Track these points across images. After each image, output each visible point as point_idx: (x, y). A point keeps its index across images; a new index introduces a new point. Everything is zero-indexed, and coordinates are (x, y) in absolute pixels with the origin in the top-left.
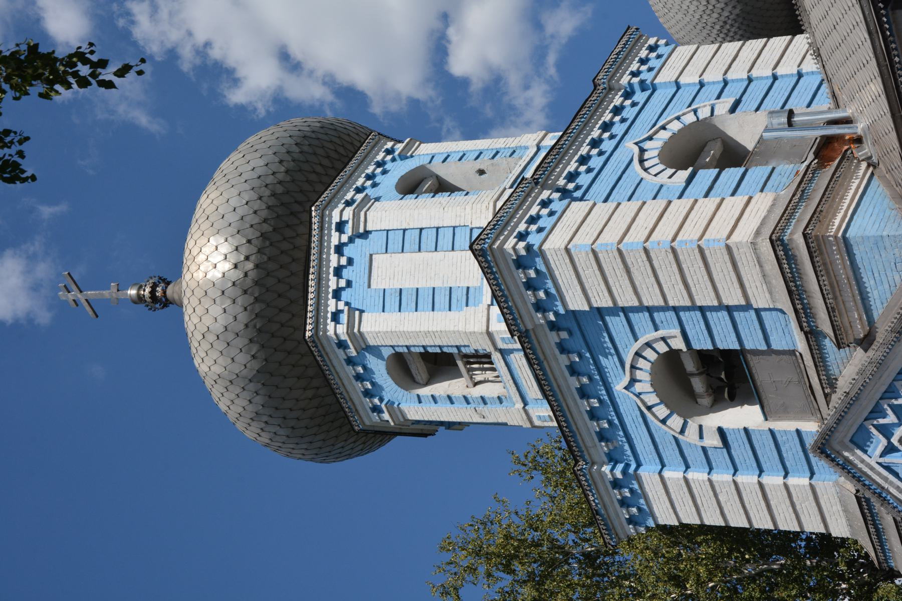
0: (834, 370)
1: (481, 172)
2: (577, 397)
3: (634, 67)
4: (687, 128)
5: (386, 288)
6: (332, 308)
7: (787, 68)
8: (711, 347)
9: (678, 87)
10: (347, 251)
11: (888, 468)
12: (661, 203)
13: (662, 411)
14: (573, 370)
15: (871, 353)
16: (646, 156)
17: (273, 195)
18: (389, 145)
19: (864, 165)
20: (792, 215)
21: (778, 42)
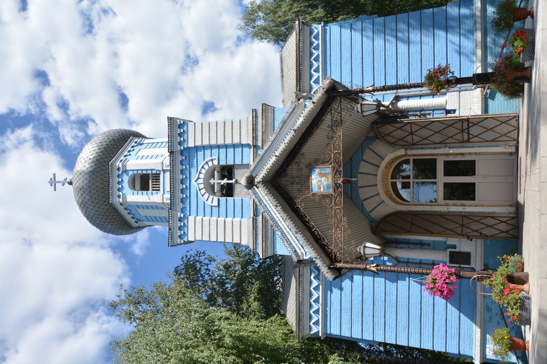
5: (137, 195)
13: (203, 191)
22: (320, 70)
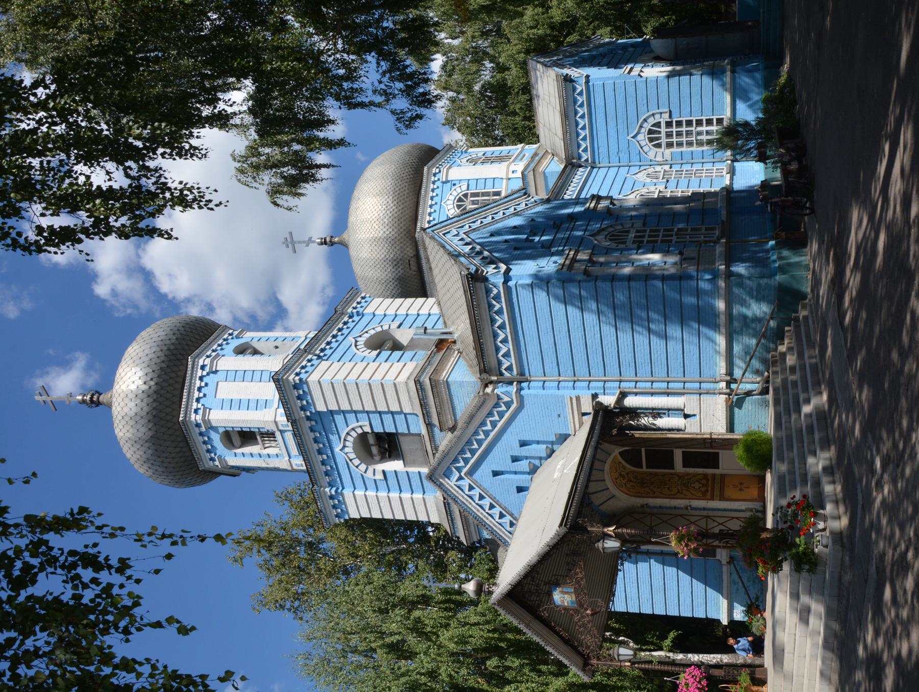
0: (438, 442)
1: (277, 347)
2: (316, 453)
3: (355, 305)
4: (377, 333)
6: (194, 407)
7: (424, 311)
8: (382, 431)
9: (374, 316)
10: (205, 379)
11: (459, 487)
12: (365, 364)
13: (357, 462)
14: (316, 441)
15: (455, 433)
16: (358, 344)
17: (169, 349)
18: (231, 331)
19: (456, 352)
20: (424, 371)
21: (420, 300)
22: (503, 299)
